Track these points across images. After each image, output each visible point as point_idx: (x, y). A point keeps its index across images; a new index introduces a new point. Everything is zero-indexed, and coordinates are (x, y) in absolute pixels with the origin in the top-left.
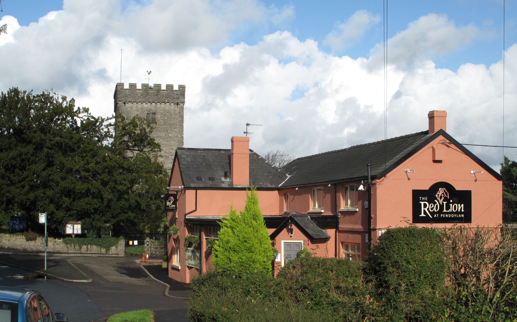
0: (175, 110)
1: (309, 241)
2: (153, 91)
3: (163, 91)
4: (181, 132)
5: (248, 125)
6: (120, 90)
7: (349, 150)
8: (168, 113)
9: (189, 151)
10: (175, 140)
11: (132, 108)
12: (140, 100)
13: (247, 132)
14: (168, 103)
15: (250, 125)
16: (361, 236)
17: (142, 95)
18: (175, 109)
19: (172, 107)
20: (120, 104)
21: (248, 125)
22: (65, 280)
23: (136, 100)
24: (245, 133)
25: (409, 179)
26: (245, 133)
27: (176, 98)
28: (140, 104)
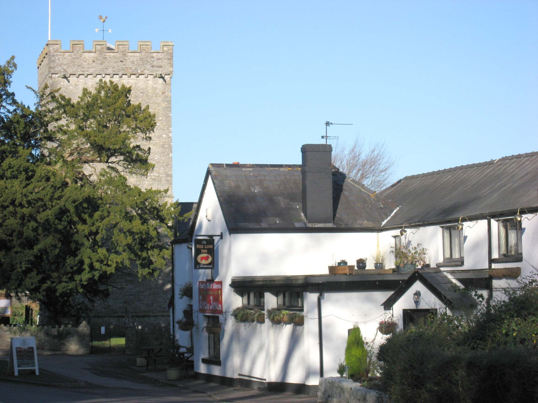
0: (156, 88)
1: (447, 309)
2: (115, 54)
3: (132, 54)
4: (167, 128)
5: (328, 124)
6: (55, 54)
7: (499, 163)
8: (142, 93)
9: (229, 168)
10: (156, 143)
11: (76, 85)
12: (91, 71)
13: (327, 137)
14: (143, 76)
15: (331, 124)
16: (123, 345)
17: (94, 61)
18: (155, 86)
19: (150, 82)
20: (55, 78)
21: (328, 124)
22: (133, 368)
23: (83, 71)
24: (323, 137)
25: (47, 45)
26: (323, 137)
27: (157, 67)
28: (91, 79)
